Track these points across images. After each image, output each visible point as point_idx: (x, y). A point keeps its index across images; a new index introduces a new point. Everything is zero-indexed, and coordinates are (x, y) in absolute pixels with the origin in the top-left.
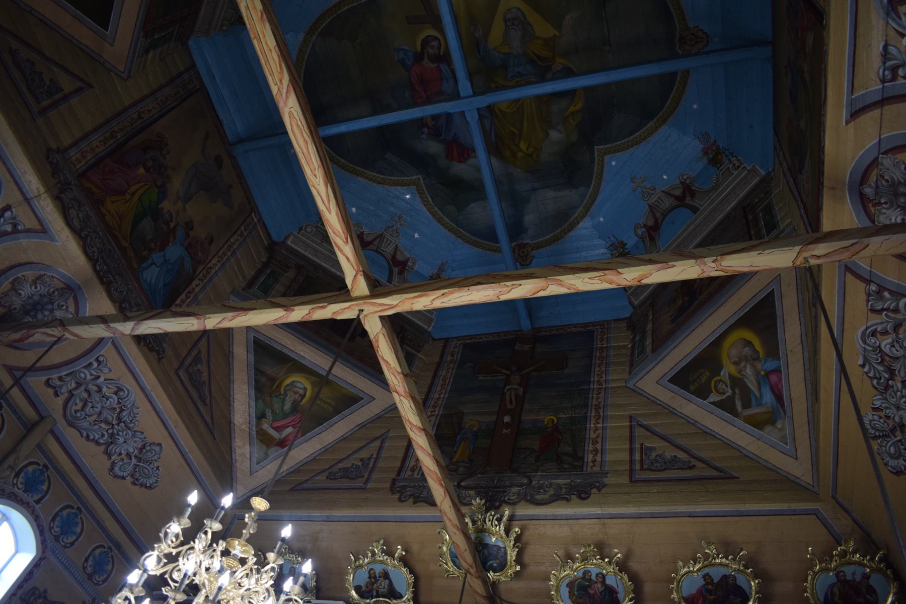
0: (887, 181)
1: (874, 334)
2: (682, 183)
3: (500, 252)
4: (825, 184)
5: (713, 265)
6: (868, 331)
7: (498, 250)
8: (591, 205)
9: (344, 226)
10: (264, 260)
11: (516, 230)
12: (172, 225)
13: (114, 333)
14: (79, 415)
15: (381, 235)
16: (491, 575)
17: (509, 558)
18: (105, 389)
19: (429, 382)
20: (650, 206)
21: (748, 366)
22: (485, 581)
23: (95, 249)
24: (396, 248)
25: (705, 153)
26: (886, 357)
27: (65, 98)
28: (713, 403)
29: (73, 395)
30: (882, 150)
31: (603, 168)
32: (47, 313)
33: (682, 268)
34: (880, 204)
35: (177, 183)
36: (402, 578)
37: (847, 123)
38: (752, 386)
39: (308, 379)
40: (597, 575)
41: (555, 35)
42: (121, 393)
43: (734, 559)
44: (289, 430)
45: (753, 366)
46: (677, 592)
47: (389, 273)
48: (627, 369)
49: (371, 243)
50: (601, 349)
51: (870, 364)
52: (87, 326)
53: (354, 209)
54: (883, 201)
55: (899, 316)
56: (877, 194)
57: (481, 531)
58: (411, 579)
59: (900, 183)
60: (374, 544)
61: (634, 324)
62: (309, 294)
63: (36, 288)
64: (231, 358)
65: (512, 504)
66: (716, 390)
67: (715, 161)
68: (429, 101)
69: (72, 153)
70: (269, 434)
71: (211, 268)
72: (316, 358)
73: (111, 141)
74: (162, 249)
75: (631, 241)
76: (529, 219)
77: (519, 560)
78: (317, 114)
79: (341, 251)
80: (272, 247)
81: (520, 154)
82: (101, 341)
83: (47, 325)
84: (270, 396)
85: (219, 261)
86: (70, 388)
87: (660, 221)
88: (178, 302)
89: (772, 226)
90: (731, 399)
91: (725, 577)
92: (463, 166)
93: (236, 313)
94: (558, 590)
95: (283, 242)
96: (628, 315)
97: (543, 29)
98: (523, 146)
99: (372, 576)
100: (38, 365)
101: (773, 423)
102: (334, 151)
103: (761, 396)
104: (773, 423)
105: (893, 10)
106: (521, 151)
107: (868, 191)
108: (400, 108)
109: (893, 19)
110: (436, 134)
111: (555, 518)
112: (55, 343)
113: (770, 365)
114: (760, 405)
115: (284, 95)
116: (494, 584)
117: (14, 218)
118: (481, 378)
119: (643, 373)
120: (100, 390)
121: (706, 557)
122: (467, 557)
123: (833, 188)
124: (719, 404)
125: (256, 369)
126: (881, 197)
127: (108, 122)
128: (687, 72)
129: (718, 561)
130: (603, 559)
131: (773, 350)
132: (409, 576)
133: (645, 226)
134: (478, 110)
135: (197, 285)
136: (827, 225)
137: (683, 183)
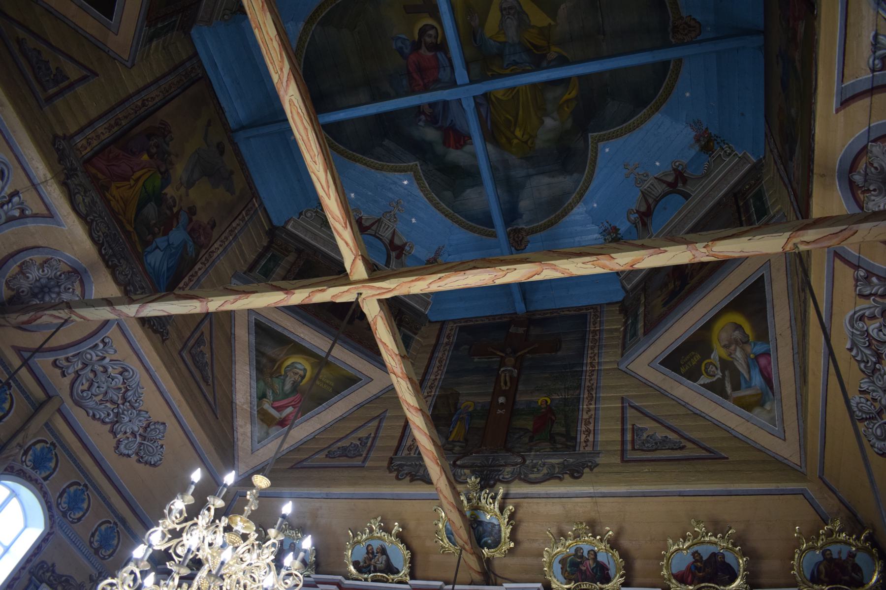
0: (876, 168)
1: (861, 318)
2: (674, 170)
3: (496, 236)
4: (815, 171)
5: (704, 250)
7: (494, 235)
8: (585, 191)
9: (343, 212)
10: (265, 244)
11: (511, 214)
12: (175, 210)
14: (85, 394)
16: (485, 551)
17: (503, 535)
18: (110, 370)
19: (426, 363)
20: (642, 192)
22: (480, 557)
23: (100, 233)
24: (394, 233)
26: (873, 341)
27: (71, 86)
28: (703, 385)
29: (79, 375)
30: (872, 138)
32: (54, 296)
33: (674, 253)
34: (868, 191)
35: (179, 171)
36: (399, 554)
37: (837, 111)
38: (742, 368)
39: (307, 360)
40: (589, 552)
42: (126, 374)
43: (723, 538)
44: (290, 410)
45: (743, 349)
46: (667, 569)
47: (388, 257)
48: (620, 352)
49: (369, 228)
50: (594, 332)
51: (858, 348)
52: (92, 309)
53: (353, 195)
54: (872, 188)
56: (866, 181)
57: (476, 508)
58: (407, 554)
60: (372, 521)
61: (626, 308)
63: (43, 271)
65: (508, 482)
66: (706, 372)
68: (426, 89)
69: (77, 139)
70: (269, 414)
71: (213, 252)
74: (166, 233)
75: (624, 226)
76: (524, 204)
77: (513, 537)
78: (317, 101)
79: (340, 236)
80: (273, 232)
81: (515, 141)
82: (106, 322)
83: (54, 307)
84: (271, 377)
85: (221, 246)
86: (77, 368)
87: (652, 207)
88: (181, 285)
89: (762, 211)
90: (721, 381)
91: (714, 555)
93: (238, 296)
94: (550, 566)
95: (284, 227)
96: (621, 299)
97: (538, 18)
98: (518, 133)
99: (370, 552)
100: (45, 346)
102: (333, 138)
106: (516, 138)
107: (858, 178)
108: (398, 96)
110: (433, 121)
111: (548, 497)
112: (62, 325)
113: (760, 348)
114: (749, 387)
115: (285, 84)
116: (489, 561)
117: (22, 203)
120: (105, 371)
121: (696, 535)
122: (462, 534)
123: (823, 176)
125: (257, 350)
127: (113, 109)
128: (679, 62)
129: (707, 539)
130: (594, 536)
131: (762, 334)
132: (406, 552)
133: (638, 212)
134: (474, 97)
135: (200, 269)
136: (816, 212)
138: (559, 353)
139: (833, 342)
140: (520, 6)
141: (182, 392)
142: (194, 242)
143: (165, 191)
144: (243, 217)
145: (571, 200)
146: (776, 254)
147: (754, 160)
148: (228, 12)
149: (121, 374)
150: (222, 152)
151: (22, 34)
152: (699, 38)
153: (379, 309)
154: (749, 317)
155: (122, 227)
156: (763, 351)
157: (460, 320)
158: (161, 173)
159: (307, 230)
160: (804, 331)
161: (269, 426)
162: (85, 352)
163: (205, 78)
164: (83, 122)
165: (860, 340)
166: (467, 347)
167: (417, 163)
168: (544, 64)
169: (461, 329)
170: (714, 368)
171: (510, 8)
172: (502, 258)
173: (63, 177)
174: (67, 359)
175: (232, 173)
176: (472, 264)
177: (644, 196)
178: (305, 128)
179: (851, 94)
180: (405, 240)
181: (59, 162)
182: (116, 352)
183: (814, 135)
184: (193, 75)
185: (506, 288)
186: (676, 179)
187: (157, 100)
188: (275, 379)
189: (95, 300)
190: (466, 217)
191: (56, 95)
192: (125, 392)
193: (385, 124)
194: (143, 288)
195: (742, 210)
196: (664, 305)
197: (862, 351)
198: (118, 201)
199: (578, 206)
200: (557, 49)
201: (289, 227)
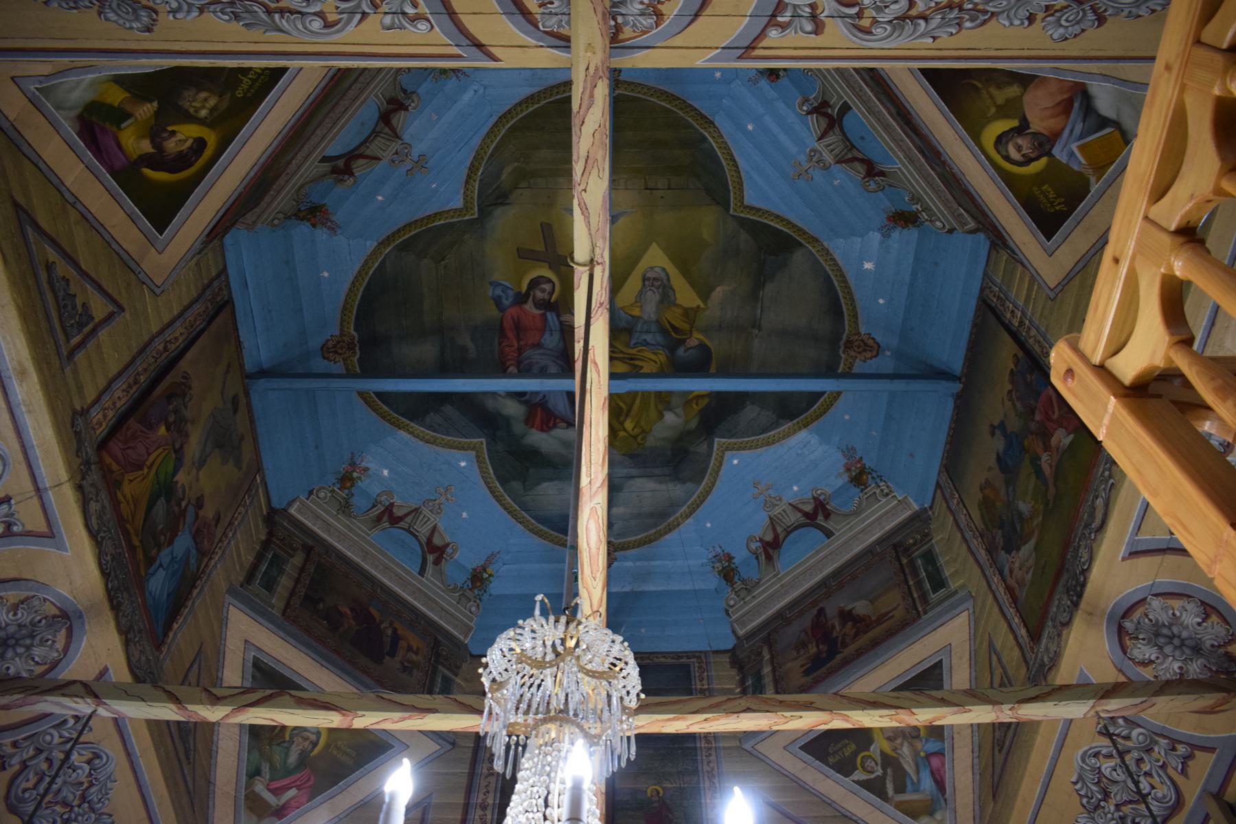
0: (1151, 620)
1: (1096, 755)
2: (814, 498)
10: (263, 538)
12: (184, 504)
14: (27, 795)
15: (416, 510)
20: (771, 518)
24: (434, 529)
25: (848, 470)
28: (857, 782)
29: (26, 767)
34: (1137, 638)
35: (193, 447)
37: (1124, 559)
38: (909, 767)
41: (698, 307)
42: (97, 761)
44: (293, 792)
45: (911, 745)
49: (401, 519)
51: (1084, 782)
53: (386, 472)
54: (1141, 636)
63: (15, 614)
66: (863, 767)
70: (262, 799)
73: (134, 388)
74: (171, 543)
75: (740, 555)
81: (622, 434)
84: (270, 745)
86: (25, 756)
87: (781, 537)
89: (938, 582)
90: (882, 779)
92: (544, 435)
93: (406, 715)
96: (730, 647)
97: (686, 296)
101: (931, 813)
103: (919, 780)
104: (931, 813)
106: (625, 430)
107: (1128, 625)
114: (916, 790)
124: (865, 785)
133: (761, 540)
140: (669, 280)
141: (168, 786)
143: (176, 479)
147: (916, 507)
148: (281, 216)
149: (89, 762)
150: (235, 410)
151: (52, 255)
156: (936, 749)
159: (318, 517)
161: (260, 816)
162: (45, 733)
170: (873, 764)
171: (655, 279)
175: (242, 438)
180: (448, 540)
184: (219, 299)
186: (816, 509)
188: (275, 747)
192: (88, 788)
195: (907, 571)
196: (807, 673)
200: (701, 337)
201: (292, 511)
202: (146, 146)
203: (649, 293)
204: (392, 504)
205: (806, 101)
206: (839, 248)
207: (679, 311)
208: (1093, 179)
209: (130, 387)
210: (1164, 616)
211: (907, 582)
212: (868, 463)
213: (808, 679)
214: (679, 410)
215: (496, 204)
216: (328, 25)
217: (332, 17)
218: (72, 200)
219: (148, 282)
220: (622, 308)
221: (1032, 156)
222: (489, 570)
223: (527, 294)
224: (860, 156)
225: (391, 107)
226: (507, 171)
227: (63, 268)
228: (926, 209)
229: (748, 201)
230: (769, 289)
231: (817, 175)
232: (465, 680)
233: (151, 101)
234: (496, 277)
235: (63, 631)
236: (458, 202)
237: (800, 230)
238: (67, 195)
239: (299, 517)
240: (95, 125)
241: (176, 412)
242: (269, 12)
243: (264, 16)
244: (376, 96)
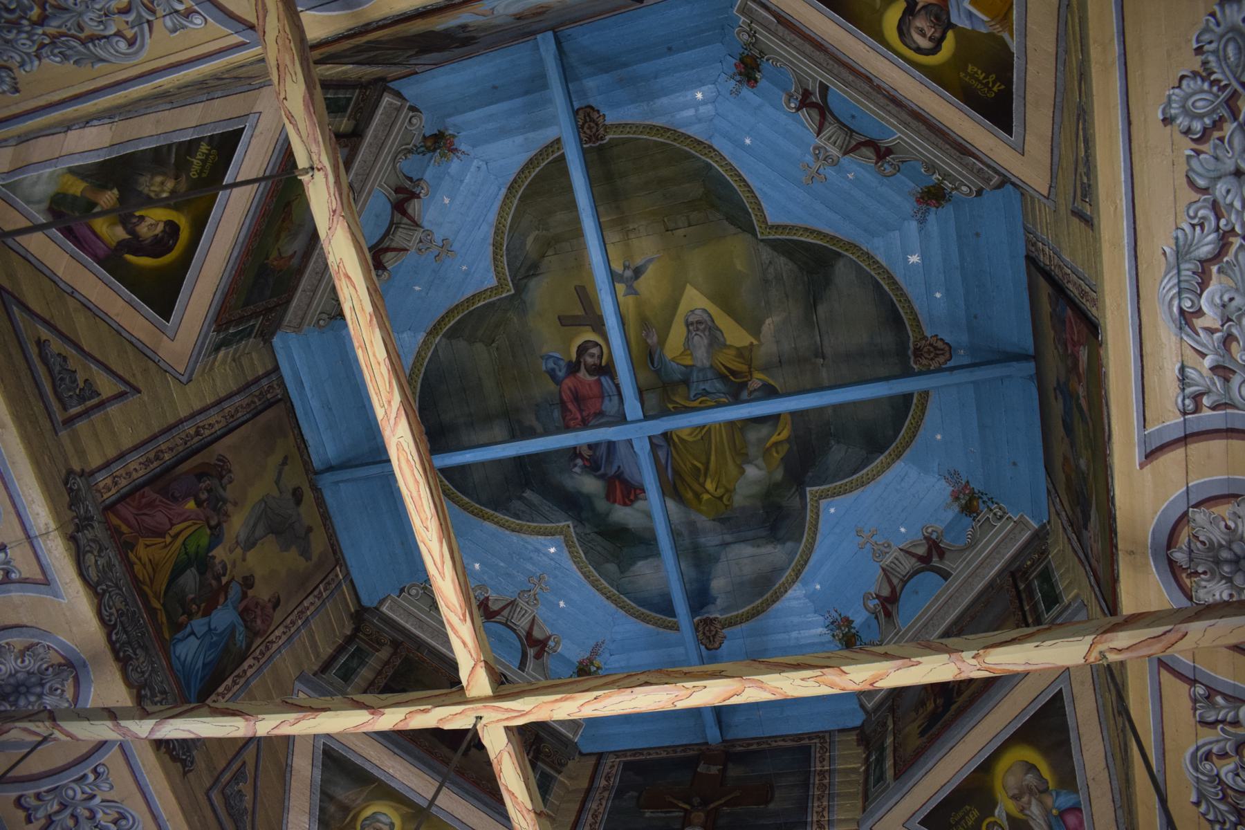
0: (1203, 543)
1: (1208, 756)
2: (925, 538)
3: (678, 629)
4: (1120, 547)
5: (974, 662)
6: (1199, 753)
7: (675, 627)
8: (803, 566)
9: (461, 598)
11: (700, 598)
12: (224, 580)
13: (124, 735)
18: (100, 815)
19: (573, 818)
20: (883, 570)
21: (1034, 802)
23: (114, 611)
25: (957, 498)
26: (1229, 792)
27: (102, 405)
29: (53, 822)
30: (1193, 502)
31: (818, 516)
32: (32, 699)
33: (930, 667)
34: (1196, 573)
35: (237, 524)
37: (1142, 466)
39: (396, 809)
41: (752, 344)
42: (124, 822)
45: (1041, 802)
47: (525, 657)
48: (860, 803)
49: (498, 613)
50: (822, 773)
51: (1208, 801)
52: (86, 723)
53: (477, 566)
54: (1200, 570)
55: (1240, 731)
56: (1191, 560)
59: (1221, 546)
61: (867, 737)
62: (404, 691)
63: (23, 661)
64: (288, 775)
67: (969, 509)
68: (585, 425)
69: (99, 477)
71: (272, 642)
72: (413, 780)
74: (207, 613)
75: (859, 618)
76: (718, 584)
78: (435, 433)
79: (456, 632)
80: (361, 615)
81: (705, 497)
82: (102, 745)
83: (30, 717)
85: (284, 633)
86: (50, 811)
87: (898, 589)
88: (221, 690)
89: (1052, 599)
92: (627, 510)
93: (301, 715)
95: (376, 608)
96: (858, 723)
97: (736, 336)
98: (710, 485)
100: (9, 775)
102: (453, 487)
105: (1186, 323)
106: (707, 492)
107: (1180, 556)
108: (547, 433)
109: (1188, 335)
110: (593, 467)
112: (40, 743)
113: (1065, 800)
115: (392, 421)
117: (8, 563)
118: (648, 815)
119: (884, 810)
120: (93, 816)
123: (1132, 553)
125: (323, 792)
126: (1198, 565)
127: (154, 438)
128: (925, 395)
131: (1067, 779)
133: (878, 597)
134: (650, 438)
135: (250, 667)
136: (1127, 606)
137: (927, 538)
138: (771, 806)
139: (1170, 805)
140: (713, 321)
142: (246, 627)
144: (320, 593)
145: (783, 579)
146: (1077, 666)
148: (324, 316)
151: (45, 333)
152: (950, 364)
153: (506, 740)
154: (1046, 752)
155: (146, 603)
156: (1070, 804)
157: (624, 753)
158: (211, 528)
159: (410, 614)
160: (1127, 774)
162: (66, 787)
163: (286, 399)
164: (111, 453)
165: (1210, 790)
166: (635, 794)
167: (569, 523)
168: (744, 395)
169: (627, 766)
171: (699, 322)
172: (685, 669)
173: (71, 529)
174: (38, 796)
175: (310, 529)
176: (643, 678)
177: (885, 574)
178: (417, 482)
179: (1158, 445)
180: (549, 632)
181: (70, 508)
182: (112, 787)
183: (1113, 497)
185: (696, 712)
186: (930, 550)
187: (217, 427)
189: (90, 709)
190: (635, 600)
191: (79, 416)
193: (527, 472)
194: (164, 692)
195: (1024, 596)
196: (922, 734)
197: (1214, 807)
198: (144, 565)
199: (794, 587)
201: (384, 609)
202: (120, 233)
203: (696, 338)
204: (487, 598)
205: (790, 96)
206: (878, 248)
207: (733, 352)
208: (1006, 36)
209: (149, 461)
210: (1217, 532)
211: (1022, 608)
212: (976, 486)
213: (924, 739)
214: (760, 461)
215: (528, 277)
216: (131, 43)
217: (129, 33)
218: (69, 290)
219: (169, 369)
220: (673, 360)
221: (937, 35)
222: (597, 662)
223: (578, 362)
224: (863, 139)
225: (401, 196)
226: (530, 240)
227: (56, 345)
228: (946, 175)
229: (770, 221)
230: (822, 309)
231: (830, 172)
232: (570, 778)
233: (111, 189)
234: (545, 350)
235: (70, 680)
236: (492, 281)
237: (833, 238)
238: (62, 285)
239: (390, 614)
240: (66, 215)
241: (209, 491)
242: (83, 43)
243: (81, 48)
244: (381, 186)
